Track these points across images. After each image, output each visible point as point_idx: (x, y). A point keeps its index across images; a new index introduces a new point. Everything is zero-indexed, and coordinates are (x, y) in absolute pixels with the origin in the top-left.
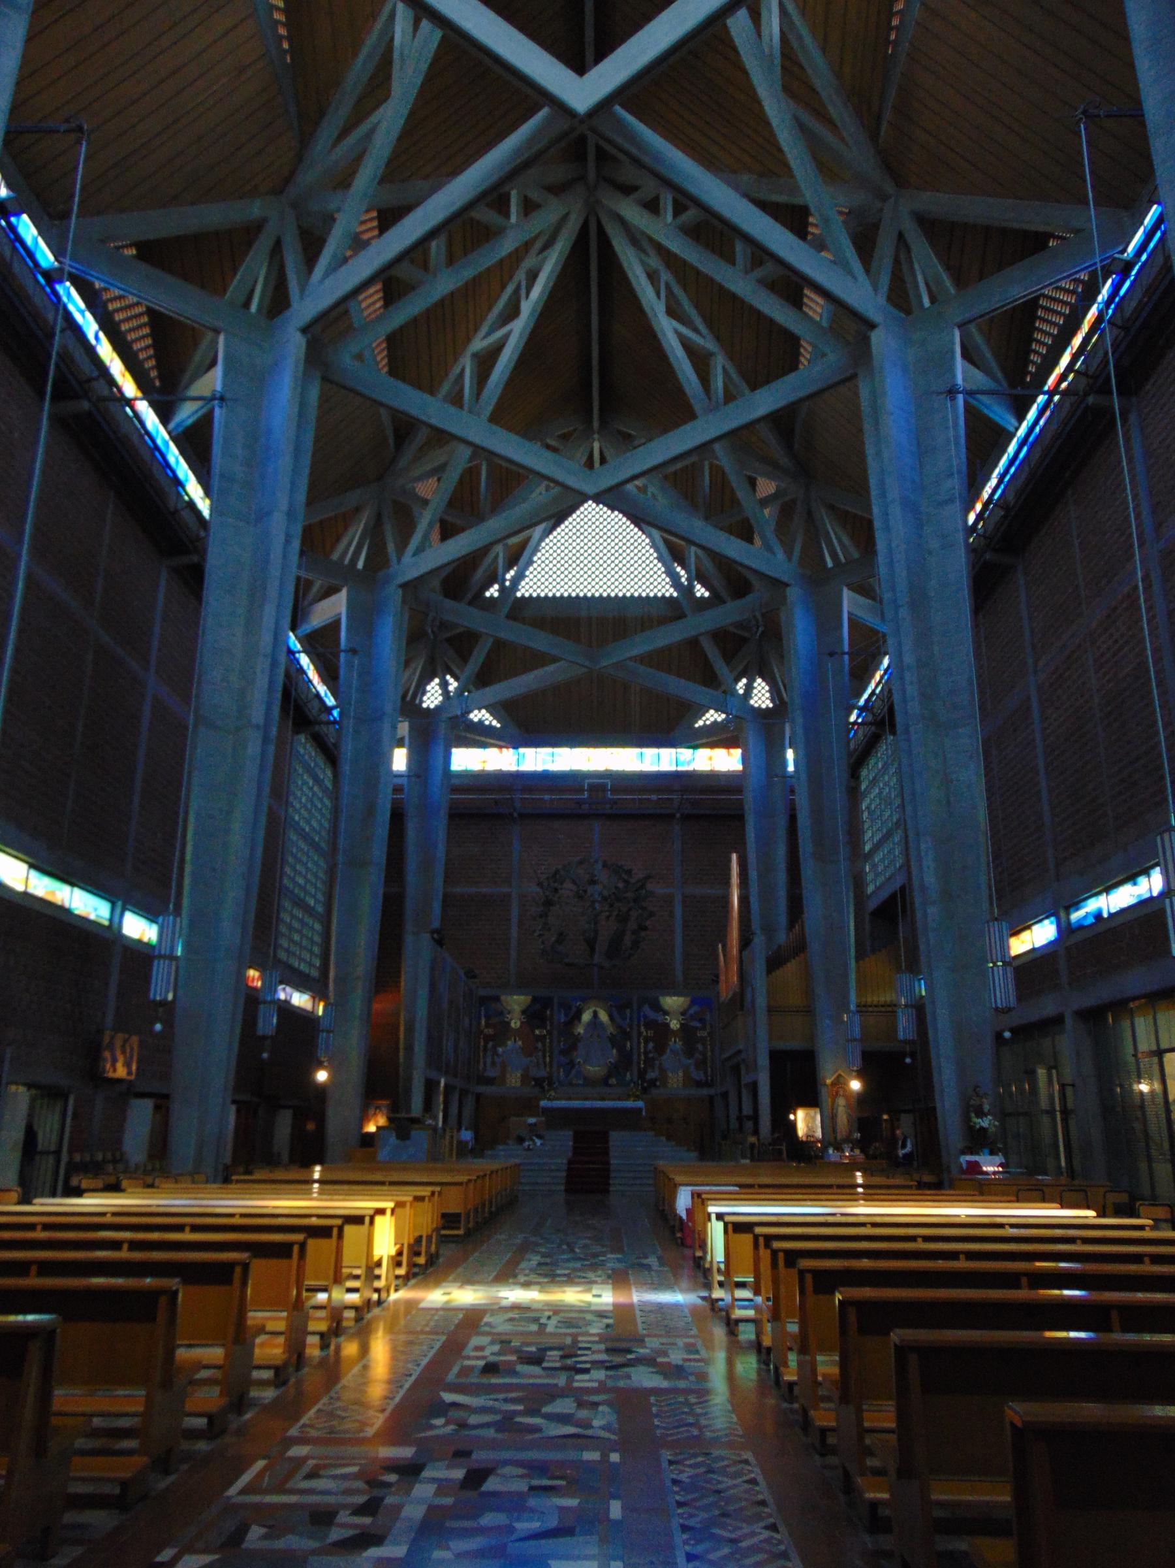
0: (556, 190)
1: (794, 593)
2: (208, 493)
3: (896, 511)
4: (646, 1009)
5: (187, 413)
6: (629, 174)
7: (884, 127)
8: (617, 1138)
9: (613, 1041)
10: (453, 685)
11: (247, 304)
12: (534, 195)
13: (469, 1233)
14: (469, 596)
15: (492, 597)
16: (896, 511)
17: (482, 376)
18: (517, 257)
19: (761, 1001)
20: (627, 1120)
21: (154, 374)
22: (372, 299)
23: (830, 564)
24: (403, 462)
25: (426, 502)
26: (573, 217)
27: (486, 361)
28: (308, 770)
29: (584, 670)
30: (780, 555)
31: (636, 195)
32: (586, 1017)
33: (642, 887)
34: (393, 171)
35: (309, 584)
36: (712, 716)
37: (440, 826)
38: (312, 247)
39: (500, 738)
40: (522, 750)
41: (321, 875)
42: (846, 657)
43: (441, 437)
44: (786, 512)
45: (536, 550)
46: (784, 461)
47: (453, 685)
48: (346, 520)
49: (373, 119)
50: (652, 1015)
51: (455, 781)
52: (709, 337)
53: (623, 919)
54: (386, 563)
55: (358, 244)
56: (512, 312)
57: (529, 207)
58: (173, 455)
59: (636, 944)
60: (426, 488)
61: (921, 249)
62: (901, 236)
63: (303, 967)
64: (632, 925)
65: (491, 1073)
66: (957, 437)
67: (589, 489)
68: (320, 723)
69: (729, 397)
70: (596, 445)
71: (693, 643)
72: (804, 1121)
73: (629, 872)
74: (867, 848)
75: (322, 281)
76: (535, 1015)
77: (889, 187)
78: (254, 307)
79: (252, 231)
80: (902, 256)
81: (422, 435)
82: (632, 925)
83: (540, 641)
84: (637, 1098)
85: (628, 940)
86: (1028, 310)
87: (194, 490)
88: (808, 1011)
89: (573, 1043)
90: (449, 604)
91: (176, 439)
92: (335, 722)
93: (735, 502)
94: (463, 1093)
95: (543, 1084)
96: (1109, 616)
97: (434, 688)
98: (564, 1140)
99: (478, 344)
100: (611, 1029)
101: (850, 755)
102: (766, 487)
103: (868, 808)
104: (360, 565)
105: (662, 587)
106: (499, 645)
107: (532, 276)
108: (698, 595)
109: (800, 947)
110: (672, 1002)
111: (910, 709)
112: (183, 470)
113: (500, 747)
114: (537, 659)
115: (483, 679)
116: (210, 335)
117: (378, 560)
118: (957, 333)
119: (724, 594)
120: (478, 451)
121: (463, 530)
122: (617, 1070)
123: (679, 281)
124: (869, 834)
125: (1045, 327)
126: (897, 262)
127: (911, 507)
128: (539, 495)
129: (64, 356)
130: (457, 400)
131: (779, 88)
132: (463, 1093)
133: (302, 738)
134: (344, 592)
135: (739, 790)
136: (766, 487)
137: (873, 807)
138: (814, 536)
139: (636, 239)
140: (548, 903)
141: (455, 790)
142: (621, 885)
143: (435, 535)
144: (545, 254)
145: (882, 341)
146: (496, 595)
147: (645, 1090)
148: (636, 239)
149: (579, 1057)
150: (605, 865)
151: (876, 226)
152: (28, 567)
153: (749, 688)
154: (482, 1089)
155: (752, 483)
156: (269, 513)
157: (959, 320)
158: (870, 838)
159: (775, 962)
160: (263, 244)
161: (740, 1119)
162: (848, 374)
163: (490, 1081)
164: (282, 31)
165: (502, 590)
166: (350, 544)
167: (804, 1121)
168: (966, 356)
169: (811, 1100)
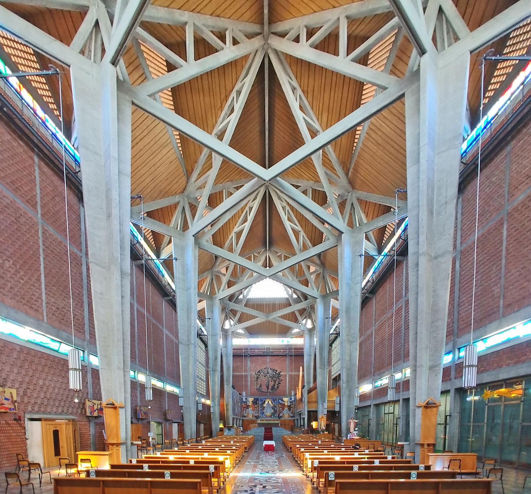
0: (250, 36)
1: (319, 301)
4: (280, 401)
7: (350, 173)
8: (274, 429)
9: (272, 407)
10: (232, 323)
11: (177, 228)
13: (248, 450)
19: (306, 401)
20: (276, 425)
21: (154, 245)
23: (328, 292)
24: (218, 263)
25: (224, 275)
27: (239, 235)
28: (199, 346)
30: (316, 290)
32: (266, 402)
33: (280, 374)
36: (296, 330)
37: (231, 358)
41: (204, 372)
47: (232, 323)
50: (281, 402)
52: (299, 226)
53: (275, 381)
56: (245, 220)
59: (278, 387)
60: (223, 271)
63: (203, 393)
64: (277, 383)
65: (245, 415)
66: (361, 266)
67: (267, 275)
71: (293, 313)
72: (314, 424)
73: (276, 371)
74: (333, 364)
75: (197, 222)
76: (255, 402)
77: (350, 189)
78: (179, 229)
79: (176, 205)
82: (277, 383)
84: (278, 421)
85: (276, 387)
86: (383, 229)
88: (316, 402)
89: (264, 408)
93: (304, 274)
94: (240, 419)
95: (257, 417)
98: (263, 429)
99: (236, 229)
100: (272, 405)
101: (330, 341)
104: (208, 294)
106: (243, 314)
107: (251, 209)
108: (294, 297)
109: (315, 388)
110: (285, 399)
111: (343, 334)
112: (164, 272)
114: (254, 317)
115: (240, 321)
117: (213, 293)
118: (364, 234)
122: (273, 414)
123: (291, 209)
124: (333, 360)
125: (389, 228)
126: (351, 214)
127: (348, 285)
130: (231, 250)
131: (321, 164)
132: (240, 419)
134: (205, 301)
140: (257, 378)
142: (274, 373)
144: (254, 202)
145: (345, 237)
146: (242, 298)
147: (280, 418)
149: (265, 411)
150: (271, 369)
153: (306, 321)
154: (243, 418)
155: (309, 268)
156: (190, 288)
158: (333, 361)
159: (310, 391)
160: (179, 209)
161: (301, 425)
162: (335, 245)
163: (245, 417)
165: (244, 296)
166: (206, 286)
167: (314, 424)
169: (316, 420)
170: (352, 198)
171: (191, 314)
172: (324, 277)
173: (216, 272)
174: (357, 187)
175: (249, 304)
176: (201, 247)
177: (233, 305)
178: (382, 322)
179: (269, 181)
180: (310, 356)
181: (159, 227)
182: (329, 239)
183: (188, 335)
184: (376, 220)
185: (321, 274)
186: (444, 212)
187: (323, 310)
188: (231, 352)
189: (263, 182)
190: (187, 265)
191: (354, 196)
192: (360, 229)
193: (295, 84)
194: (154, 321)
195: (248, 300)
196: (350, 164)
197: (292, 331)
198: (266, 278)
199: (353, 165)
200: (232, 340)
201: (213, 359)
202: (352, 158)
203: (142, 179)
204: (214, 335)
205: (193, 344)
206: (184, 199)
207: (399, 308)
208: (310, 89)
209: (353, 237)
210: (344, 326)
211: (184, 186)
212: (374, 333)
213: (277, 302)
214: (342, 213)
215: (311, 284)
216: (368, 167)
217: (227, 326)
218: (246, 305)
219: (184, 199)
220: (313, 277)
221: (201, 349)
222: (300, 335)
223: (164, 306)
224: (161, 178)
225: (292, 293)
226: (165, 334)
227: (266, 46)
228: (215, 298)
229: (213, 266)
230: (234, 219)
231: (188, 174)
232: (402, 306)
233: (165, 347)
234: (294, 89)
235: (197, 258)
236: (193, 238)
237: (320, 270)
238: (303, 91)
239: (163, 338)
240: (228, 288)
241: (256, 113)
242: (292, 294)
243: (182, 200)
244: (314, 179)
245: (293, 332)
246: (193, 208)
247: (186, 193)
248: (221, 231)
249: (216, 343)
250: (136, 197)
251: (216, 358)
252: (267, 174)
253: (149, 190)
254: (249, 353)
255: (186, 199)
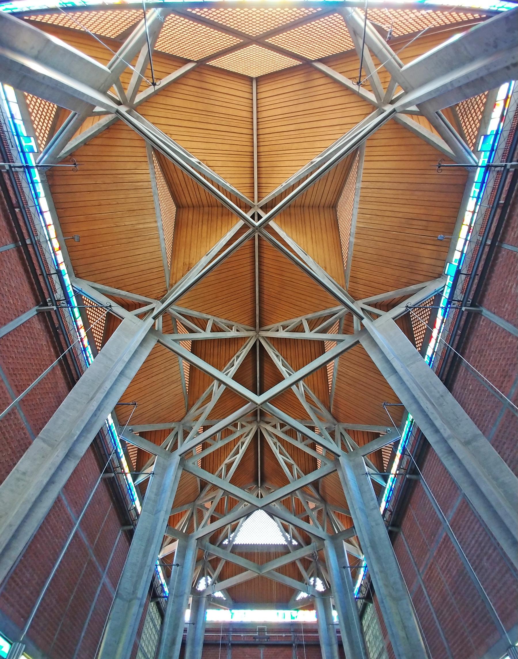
0: (250, 423)
1: (327, 543)
2: (141, 505)
3: (358, 511)
5: (141, 479)
6: (268, 419)
7: (332, 409)
10: (210, 580)
11: (165, 448)
12: (244, 423)
14: (218, 544)
15: (225, 544)
16: (358, 511)
17: (228, 470)
18: (239, 438)
21: (135, 467)
22: (200, 447)
23: (337, 532)
24: (202, 495)
25: (208, 509)
26: (253, 429)
27: (229, 466)
28: (152, 620)
29: (257, 574)
30: (321, 528)
31: (270, 424)
34: (210, 417)
35: (167, 537)
36: (303, 595)
37: (200, 649)
38: (186, 434)
39: (225, 605)
40: (233, 611)
42: (349, 569)
43: (215, 487)
44: (320, 513)
45: (241, 526)
46: (317, 496)
47: (210, 580)
48: (181, 515)
49: (206, 405)
51: (207, 627)
54: (193, 531)
55: (198, 434)
56: (237, 452)
57: (242, 426)
58: (134, 490)
60: (208, 505)
61: (347, 436)
62: (341, 433)
68: (160, 597)
69: (299, 477)
70: (259, 492)
71: (294, 563)
77: (336, 422)
78: (167, 449)
79: (171, 430)
80: (343, 439)
81: (208, 488)
83: (241, 562)
86: (379, 454)
87: (137, 503)
90: (212, 546)
91: (135, 487)
92: (166, 597)
96: (439, 551)
97: (203, 581)
99: (227, 461)
102: (312, 505)
103: (369, 640)
104: (184, 532)
105: (282, 541)
106: (227, 563)
107: (243, 443)
112: (136, 496)
113: (225, 609)
114: (242, 570)
115: (221, 578)
116: (154, 456)
117: (190, 529)
119: (303, 544)
120: (226, 492)
121: (218, 519)
126: (342, 440)
127: (362, 510)
128: (241, 509)
129: (112, 461)
130: (220, 476)
133: (152, 603)
135: (316, 631)
136: (312, 505)
137: (371, 640)
138: (330, 521)
139: (270, 434)
141: (207, 631)
143: (209, 521)
145: (342, 460)
146: (227, 543)
148: (270, 434)
151: (334, 431)
152: (77, 529)
153: (315, 581)
156: (160, 511)
157: (362, 454)
160: (173, 433)
164: (187, 388)
165: (229, 541)
168: (367, 465)
170: (339, 428)
171: (150, 546)
172: (327, 514)
173: (198, 505)
174: (342, 421)
175: (236, 549)
176: (187, 469)
177: (215, 551)
178: (429, 566)
179: (261, 404)
180: (330, 645)
181: (146, 446)
182: (325, 464)
183: (137, 581)
184: (370, 444)
185: (324, 509)
186: (445, 403)
187: (336, 558)
188: (201, 636)
189: (256, 406)
190: (165, 484)
191: (341, 427)
192: (357, 453)
193: (277, 353)
194: (94, 559)
195: (235, 547)
196: (330, 403)
197: (297, 595)
198: (258, 509)
199: (332, 402)
200: (205, 613)
201: (169, 645)
202: (330, 398)
203: (145, 405)
204: (179, 595)
205: (139, 599)
206: (179, 426)
207: (444, 539)
208: (289, 357)
209: (351, 461)
210: (376, 569)
211: (182, 417)
212: (423, 587)
213: (273, 550)
214: (333, 439)
215: (313, 521)
216: (345, 402)
217: (202, 586)
218: (232, 551)
219: (179, 426)
220: (315, 514)
221: (155, 625)
222: (308, 605)
223: (120, 535)
224: (163, 407)
225: (290, 538)
226: (101, 585)
227: (259, 427)
228: (192, 537)
229: (197, 497)
230: (226, 448)
231: (189, 407)
232: (447, 534)
233: (93, 607)
234: (277, 356)
235: (179, 479)
236: (179, 458)
237: (322, 506)
238: (284, 358)
239: (96, 590)
240: (211, 523)
241: (250, 372)
242: (291, 540)
243: (177, 427)
244: (300, 417)
245: (297, 599)
246: (201, 518)
247: (183, 421)
248: (212, 457)
249: (179, 614)
250: (131, 403)
251: (173, 642)
252: (259, 399)
253: (147, 415)
254: (231, 639)
255: (181, 426)
